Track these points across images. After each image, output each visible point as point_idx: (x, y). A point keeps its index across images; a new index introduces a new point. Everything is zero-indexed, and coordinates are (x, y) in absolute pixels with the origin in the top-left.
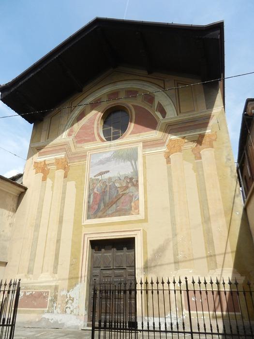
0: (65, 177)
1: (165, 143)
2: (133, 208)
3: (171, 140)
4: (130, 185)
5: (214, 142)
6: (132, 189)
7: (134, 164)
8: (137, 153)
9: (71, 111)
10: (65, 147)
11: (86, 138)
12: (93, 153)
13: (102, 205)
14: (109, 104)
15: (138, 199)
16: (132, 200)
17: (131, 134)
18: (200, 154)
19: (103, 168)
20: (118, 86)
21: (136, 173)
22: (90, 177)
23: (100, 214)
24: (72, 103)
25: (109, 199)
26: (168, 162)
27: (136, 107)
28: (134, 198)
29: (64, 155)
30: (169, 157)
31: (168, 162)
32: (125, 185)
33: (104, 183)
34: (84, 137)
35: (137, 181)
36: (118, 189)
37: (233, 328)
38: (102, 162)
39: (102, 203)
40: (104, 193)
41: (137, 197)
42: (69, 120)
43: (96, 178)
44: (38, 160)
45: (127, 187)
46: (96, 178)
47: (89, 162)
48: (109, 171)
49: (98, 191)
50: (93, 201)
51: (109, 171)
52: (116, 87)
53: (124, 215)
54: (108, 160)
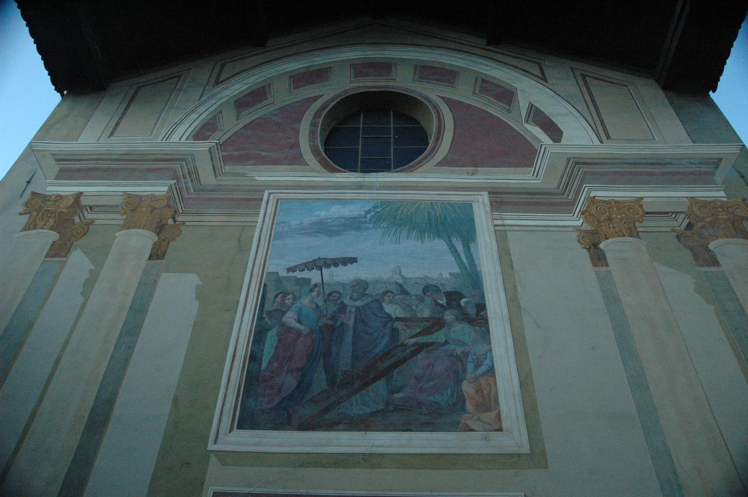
0: (157, 254)
1: (573, 203)
2: (469, 406)
3: (593, 200)
4: (449, 316)
5: (54, 236)
6: (460, 331)
7: (460, 248)
8: (472, 221)
9: (217, 83)
10: (176, 165)
11: (263, 154)
12: (293, 196)
13: (320, 381)
14: (357, 85)
15: (491, 371)
16: (464, 371)
17: (440, 164)
18: (710, 251)
19: (331, 248)
20: (387, 52)
21: (475, 280)
22: (271, 267)
23: (307, 411)
24: (223, 66)
25: (355, 357)
26: (598, 258)
27: (452, 104)
28: (470, 367)
29: (166, 189)
30: (595, 246)
31: (598, 258)
32: (426, 313)
33: (333, 295)
34: (259, 142)
35: (481, 307)
36: (398, 325)
37: (129, 99)
38: (323, 228)
39: (320, 368)
40: (330, 332)
41: (487, 362)
42: (205, 102)
43: (298, 274)
44: (50, 188)
45: (437, 324)
46: (298, 274)
47: (268, 222)
48: (353, 260)
49: (299, 322)
50: (276, 357)
51: (353, 260)
52: (382, 52)
53: (429, 426)
54: (353, 224)
